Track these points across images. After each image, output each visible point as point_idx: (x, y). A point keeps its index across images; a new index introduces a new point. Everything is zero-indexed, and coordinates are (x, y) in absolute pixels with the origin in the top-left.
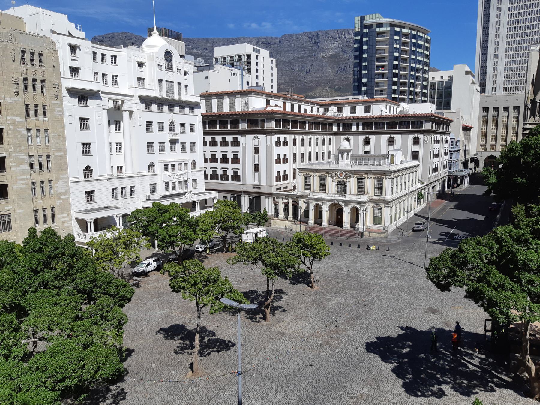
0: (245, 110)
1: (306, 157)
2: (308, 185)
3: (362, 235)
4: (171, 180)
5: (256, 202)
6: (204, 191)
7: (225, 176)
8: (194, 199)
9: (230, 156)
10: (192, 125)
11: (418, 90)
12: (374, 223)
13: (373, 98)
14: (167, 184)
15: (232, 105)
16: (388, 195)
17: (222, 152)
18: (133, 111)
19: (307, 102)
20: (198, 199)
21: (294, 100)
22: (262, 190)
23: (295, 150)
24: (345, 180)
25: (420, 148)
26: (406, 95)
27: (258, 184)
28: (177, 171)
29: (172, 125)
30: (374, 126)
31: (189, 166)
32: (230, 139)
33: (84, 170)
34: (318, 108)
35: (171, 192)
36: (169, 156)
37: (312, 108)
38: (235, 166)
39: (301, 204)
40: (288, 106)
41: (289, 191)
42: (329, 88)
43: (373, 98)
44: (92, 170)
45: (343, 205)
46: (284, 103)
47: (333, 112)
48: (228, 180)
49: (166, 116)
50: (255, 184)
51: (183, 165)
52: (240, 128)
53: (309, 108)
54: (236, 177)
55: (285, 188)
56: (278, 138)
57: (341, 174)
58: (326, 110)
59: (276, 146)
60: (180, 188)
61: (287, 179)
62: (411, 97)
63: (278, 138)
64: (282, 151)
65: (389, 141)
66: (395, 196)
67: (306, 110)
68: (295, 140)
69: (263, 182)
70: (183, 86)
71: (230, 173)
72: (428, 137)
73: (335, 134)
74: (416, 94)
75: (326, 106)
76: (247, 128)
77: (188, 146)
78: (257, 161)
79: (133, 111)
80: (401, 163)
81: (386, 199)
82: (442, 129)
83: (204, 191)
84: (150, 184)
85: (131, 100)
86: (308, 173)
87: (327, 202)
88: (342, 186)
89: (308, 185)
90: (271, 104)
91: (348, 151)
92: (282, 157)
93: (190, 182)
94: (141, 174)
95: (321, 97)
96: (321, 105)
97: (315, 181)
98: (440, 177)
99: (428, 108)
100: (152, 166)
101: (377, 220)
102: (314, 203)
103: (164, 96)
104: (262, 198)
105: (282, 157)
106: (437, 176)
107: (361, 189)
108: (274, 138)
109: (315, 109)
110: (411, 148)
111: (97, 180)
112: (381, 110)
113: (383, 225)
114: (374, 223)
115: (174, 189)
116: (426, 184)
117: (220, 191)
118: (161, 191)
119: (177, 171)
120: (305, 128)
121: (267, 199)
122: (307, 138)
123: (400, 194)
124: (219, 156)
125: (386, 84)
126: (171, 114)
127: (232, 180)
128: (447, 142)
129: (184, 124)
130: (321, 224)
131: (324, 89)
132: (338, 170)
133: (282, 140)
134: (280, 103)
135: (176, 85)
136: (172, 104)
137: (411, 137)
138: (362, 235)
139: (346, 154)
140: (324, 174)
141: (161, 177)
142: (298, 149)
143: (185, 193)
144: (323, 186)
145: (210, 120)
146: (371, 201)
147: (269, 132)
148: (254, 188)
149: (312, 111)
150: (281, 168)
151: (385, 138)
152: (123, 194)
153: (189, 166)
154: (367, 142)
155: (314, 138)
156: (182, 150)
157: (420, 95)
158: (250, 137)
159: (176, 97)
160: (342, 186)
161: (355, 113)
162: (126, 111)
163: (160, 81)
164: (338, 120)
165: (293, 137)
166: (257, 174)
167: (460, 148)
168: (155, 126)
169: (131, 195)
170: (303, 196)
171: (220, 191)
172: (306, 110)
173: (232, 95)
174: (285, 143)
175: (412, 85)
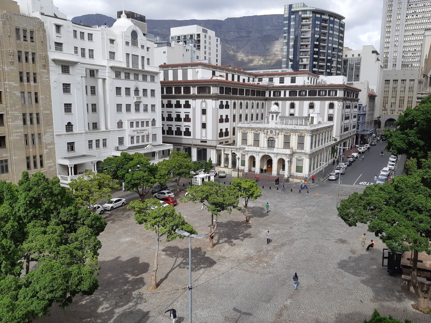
1: (243, 117)
4: (135, 134)
5: (202, 153)
6: (162, 144)
12: (297, 171)
13: (298, 71)
14: (132, 138)
15: (185, 74)
18: (105, 79)
19: (246, 74)
22: (208, 144)
24: (275, 137)
26: (324, 69)
27: (205, 138)
28: (140, 128)
29: (137, 91)
30: (296, 93)
31: (150, 123)
32: (183, 102)
34: (254, 79)
35: (135, 144)
36: (134, 116)
40: (230, 76)
45: (272, 156)
46: (227, 75)
47: (265, 81)
48: (173, 134)
49: (132, 84)
50: (203, 138)
52: (191, 94)
53: (246, 78)
54: (187, 133)
56: (222, 102)
57: (271, 132)
59: (220, 108)
60: (143, 141)
62: (328, 71)
63: (222, 102)
64: (224, 112)
65: (310, 106)
67: (244, 80)
79: (105, 79)
81: (306, 152)
83: (162, 144)
85: (104, 70)
88: (271, 143)
92: (224, 117)
99: (338, 80)
102: (250, 155)
103: (131, 67)
104: (208, 150)
106: (347, 134)
107: (287, 144)
109: (251, 79)
110: (327, 112)
111: (76, 134)
114: (297, 171)
115: (138, 142)
118: (127, 143)
119: (140, 128)
124: (174, 116)
128: (356, 107)
133: (224, 103)
137: (327, 103)
141: (127, 132)
144: (256, 142)
147: (215, 97)
148: (202, 142)
149: (249, 81)
150: (224, 126)
151: (306, 103)
152: (98, 146)
153: (150, 123)
154: (292, 106)
158: (199, 101)
159: (140, 68)
160: (271, 143)
163: (128, 55)
166: (204, 130)
172: (244, 80)
173: (184, 66)
174: (227, 106)
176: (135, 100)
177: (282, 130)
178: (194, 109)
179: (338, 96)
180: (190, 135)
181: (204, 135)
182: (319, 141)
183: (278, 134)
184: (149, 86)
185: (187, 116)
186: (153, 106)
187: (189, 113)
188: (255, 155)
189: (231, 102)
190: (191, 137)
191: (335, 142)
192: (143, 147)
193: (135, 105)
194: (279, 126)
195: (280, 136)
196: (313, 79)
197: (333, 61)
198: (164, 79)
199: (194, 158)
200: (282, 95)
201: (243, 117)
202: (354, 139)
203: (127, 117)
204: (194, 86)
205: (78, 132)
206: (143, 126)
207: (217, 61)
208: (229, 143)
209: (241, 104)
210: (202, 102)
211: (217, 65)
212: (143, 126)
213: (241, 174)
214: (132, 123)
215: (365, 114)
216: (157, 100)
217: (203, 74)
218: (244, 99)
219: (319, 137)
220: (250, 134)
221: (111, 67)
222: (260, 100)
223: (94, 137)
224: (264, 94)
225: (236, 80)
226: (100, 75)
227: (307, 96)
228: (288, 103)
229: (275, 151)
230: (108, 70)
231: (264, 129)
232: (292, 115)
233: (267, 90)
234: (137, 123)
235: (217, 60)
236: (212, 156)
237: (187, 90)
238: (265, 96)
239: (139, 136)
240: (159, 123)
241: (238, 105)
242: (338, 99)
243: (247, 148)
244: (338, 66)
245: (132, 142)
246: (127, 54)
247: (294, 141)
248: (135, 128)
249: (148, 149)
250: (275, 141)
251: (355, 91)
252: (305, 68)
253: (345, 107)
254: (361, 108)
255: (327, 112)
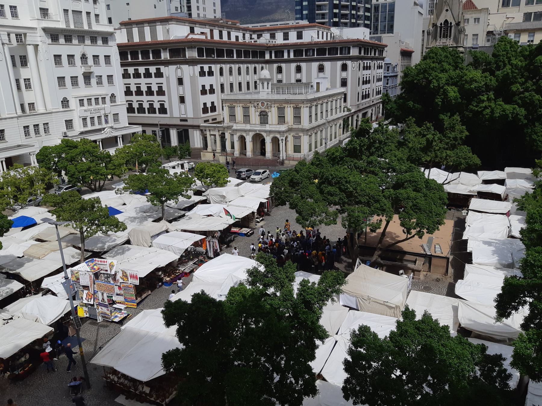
0: (167, 39)
1: (244, 86)
2: (232, 116)
3: (282, 163)
4: (89, 115)
5: (184, 136)
6: (128, 125)
7: (152, 110)
8: (115, 134)
9: (155, 88)
10: (107, 57)
11: (361, 13)
12: (295, 152)
13: (315, 22)
14: (84, 119)
15: (154, 33)
16: (305, 123)
17: (146, 84)
18: (38, 45)
19: (238, 29)
20: (119, 133)
21: (223, 27)
22: (189, 123)
23: (222, 80)
24: (267, 110)
25: (348, 75)
26: (348, 19)
27: (185, 116)
28: (94, 106)
29: (84, 57)
30: (302, 52)
31: (108, 99)
32: (153, 70)
33: (62, 102)
34: (251, 35)
35: (89, 128)
36: (83, 91)
37: (244, 35)
38: (161, 98)
39: (227, 136)
40: (216, 33)
41: (218, 123)
42: (290, 10)
43: (315, 22)
44: (68, 101)
45: (264, 134)
46: (212, 31)
47: (265, 39)
48: (145, 113)
49: (76, 49)
50: (182, 116)
51: (100, 100)
52: (163, 58)
53: (240, 35)
54: (163, 110)
55: (213, 120)
56: (202, 68)
57: (263, 104)
58: (259, 36)
59: (200, 76)
60: (100, 123)
61: (215, 111)
62: (353, 21)
63: (202, 68)
64: (207, 81)
65: (319, 69)
66: (314, 124)
67: (237, 38)
68: (221, 69)
69: (190, 115)
70: (93, 16)
71: (157, 106)
72: (356, 64)
73: (267, 62)
74: (358, 17)
75: (259, 33)
76: (169, 58)
77: (105, 80)
78: (181, 93)
79: (38, 45)
80: (327, 89)
81: (304, 127)
82: (373, 55)
83: (128, 125)
84: (66, 121)
85: (35, 33)
86: (231, 104)
87: (250, 133)
88: (264, 117)
89: (232, 116)
90: (196, 33)
91: (268, 80)
92: (208, 88)
93: (111, 118)
94: (54, 111)
95: (282, 20)
96: (254, 31)
97: (239, 112)
98: (372, 104)
99: (361, 33)
100: (65, 103)
101: (297, 149)
102: (239, 134)
103: (72, 27)
105: (208, 88)
106: (368, 102)
107: (282, 119)
108: (198, 68)
109: (247, 36)
110: (340, 75)
111: (6, 119)
112: (311, 36)
113: (302, 153)
114: (295, 152)
115: (93, 124)
116: (353, 111)
117: (143, 125)
118: (78, 127)
119: (94, 106)
120: (233, 57)
121: (195, 132)
122: (235, 67)
123: (320, 122)
124: (144, 89)
125: (328, 7)
126: (82, 46)
127: (160, 113)
128: (380, 67)
129: (98, 56)
130: (246, 155)
131: (284, 12)
132: (258, 101)
133: (206, 69)
134: (207, 31)
135: (84, 15)
136: (82, 36)
137: (339, 63)
138: (282, 163)
139: (266, 84)
140: (246, 105)
141: (76, 113)
142: (226, 79)
143: (104, 129)
144: (247, 117)
145: (123, 51)
146: (290, 130)
147: (192, 62)
148: (181, 120)
149: (244, 37)
150: (208, 99)
151: (315, 65)
152: (37, 132)
153: (108, 99)
154: (299, 69)
155: (226, 68)
156: (98, 83)
157: (363, 18)
158: (172, 68)
159: (86, 27)
160: (264, 117)
161: (288, 39)
162: (29, 45)
163: (66, 11)
164: (270, 47)
165: (219, 66)
166: (182, 106)
167: (398, 73)
168: (64, 59)
169: (36, 134)
170: (229, 128)
171: (143, 125)
172: (237, 38)
173: (152, 22)
174: (211, 73)
175: (354, 8)
176: (83, 70)
177: (275, 101)
178: (168, 78)
179: (351, 55)
180: (167, 113)
181: (183, 112)
182: (316, 114)
183: (271, 107)
184: (100, 50)
185: (160, 88)
186: (110, 77)
187: (162, 84)
188: (244, 135)
189: (216, 68)
190: (168, 115)
191: (348, 113)
192: (99, 130)
193: (84, 77)
194: (271, 97)
195: (273, 109)
196: (320, 33)
197: (359, 8)
198: (128, 41)
199: (174, 141)
200: (286, 56)
201: (244, 86)
202: (379, 108)
203: (73, 94)
204: (165, 49)
205: (7, 116)
206: (97, 103)
207: (215, 13)
208: (218, 120)
209: (239, 69)
210: (177, 68)
211: (215, 17)
212: (97, 103)
213: (229, 159)
214: (81, 101)
215: (396, 76)
216: (116, 69)
217: (179, 32)
218: (234, 62)
219: (322, 109)
220: (289, 109)
221: (45, 30)
222: (258, 62)
223: (30, 122)
224: (263, 54)
225: (225, 38)
226: (29, 39)
227: (315, 56)
228: (293, 65)
229: (268, 127)
230: (40, 33)
231: (255, 101)
232: (299, 81)
233: (267, 50)
234: (89, 100)
235: (215, 10)
236: (196, 140)
237: (157, 54)
238: (264, 57)
239: (94, 117)
240: (121, 99)
241: (251, 70)
242: (352, 59)
243: (235, 127)
244: (367, 14)
245: (85, 125)
246: (64, 10)
247: (289, 113)
248: (86, 107)
249: (107, 134)
250: (268, 116)
251: (377, 47)
252: (323, 18)
253: (376, 68)
254: (390, 68)
255: (340, 75)
